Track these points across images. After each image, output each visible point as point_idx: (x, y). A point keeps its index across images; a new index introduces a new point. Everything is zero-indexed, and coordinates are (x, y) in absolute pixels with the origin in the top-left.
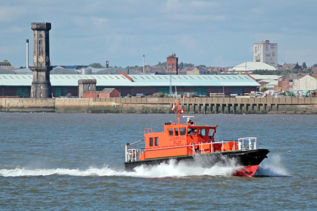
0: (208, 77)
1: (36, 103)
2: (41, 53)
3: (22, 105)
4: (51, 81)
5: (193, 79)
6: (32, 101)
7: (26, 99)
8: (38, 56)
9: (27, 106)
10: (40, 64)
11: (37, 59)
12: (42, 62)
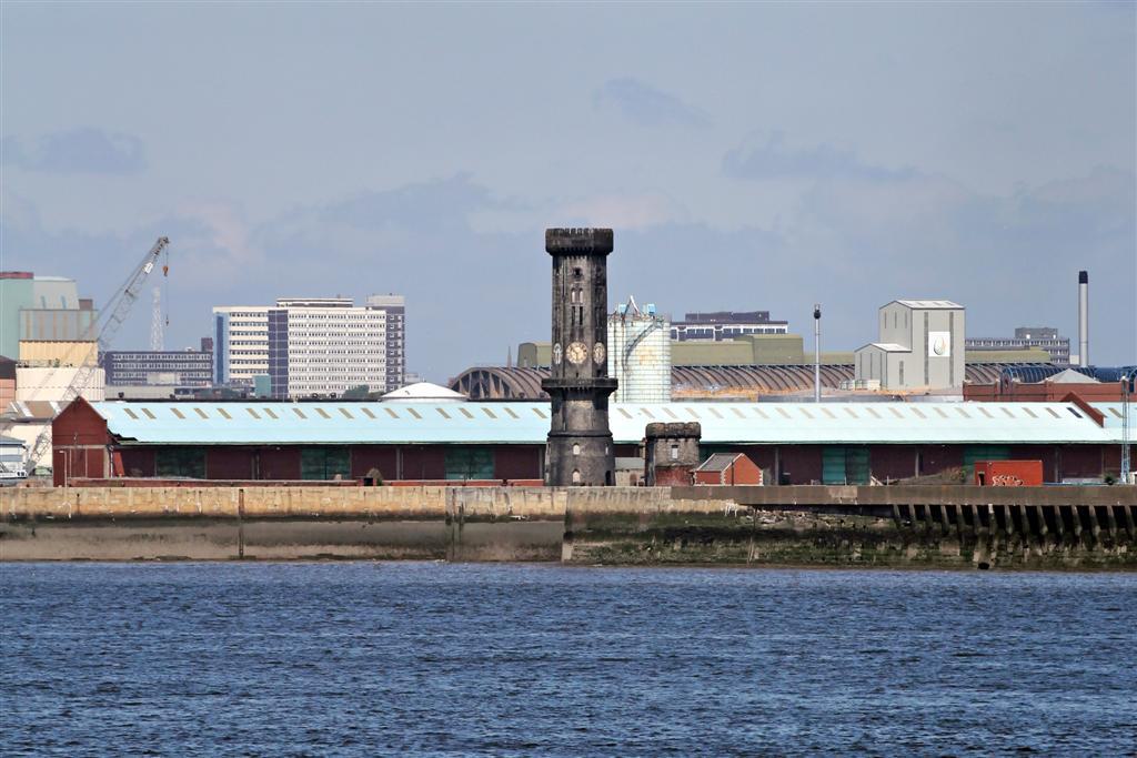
0: (1112, 409)
1: (552, 503)
2: (577, 334)
3: (506, 511)
4: (613, 427)
5: (1034, 416)
6: (540, 496)
7: (519, 491)
8: (567, 342)
9: (522, 512)
10: (574, 370)
11: (564, 353)
12: (581, 362)
